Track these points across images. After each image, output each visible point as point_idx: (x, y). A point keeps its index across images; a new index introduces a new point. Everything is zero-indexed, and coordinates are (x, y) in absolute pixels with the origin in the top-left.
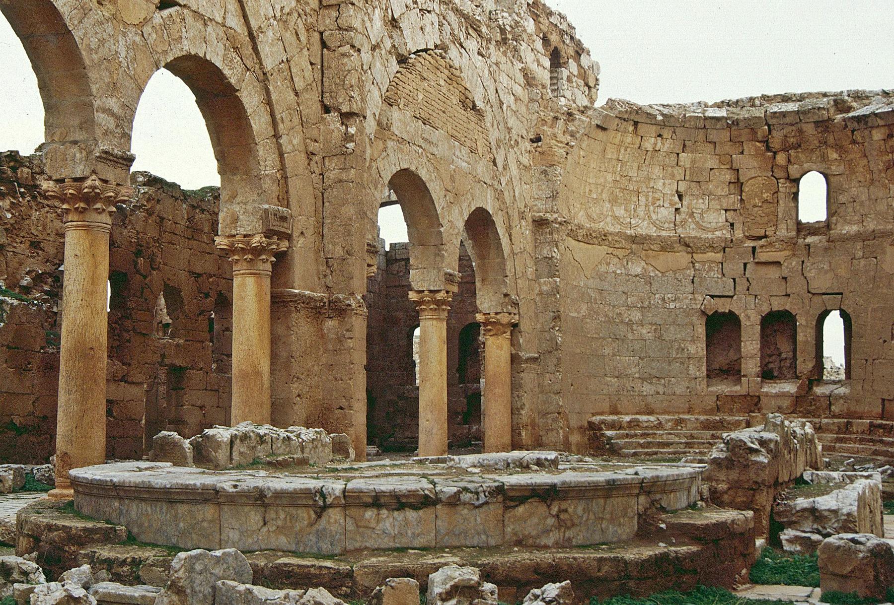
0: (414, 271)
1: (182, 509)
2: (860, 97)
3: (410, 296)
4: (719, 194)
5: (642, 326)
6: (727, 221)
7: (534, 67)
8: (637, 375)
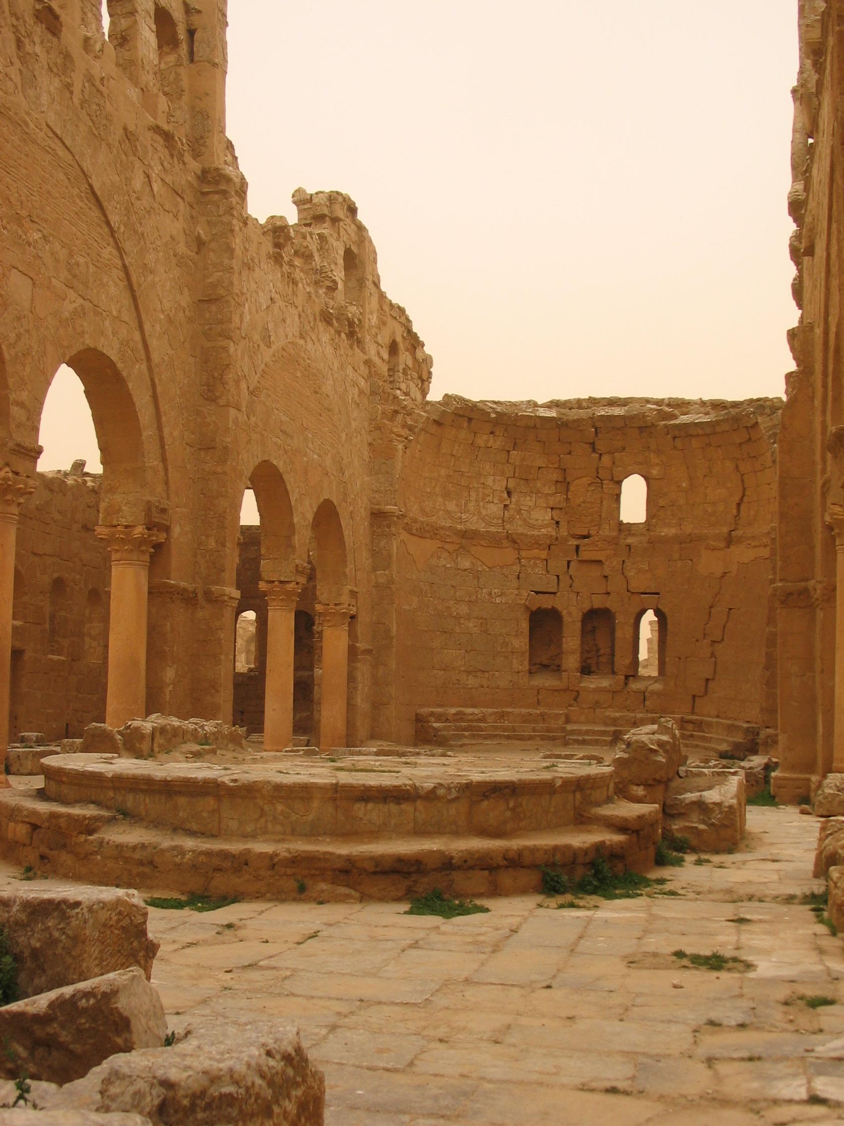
0: (265, 561)
1: (182, 801)
2: (681, 405)
3: (260, 586)
4: (546, 492)
5: (469, 620)
6: (552, 519)
7: (376, 359)
8: (462, 669)
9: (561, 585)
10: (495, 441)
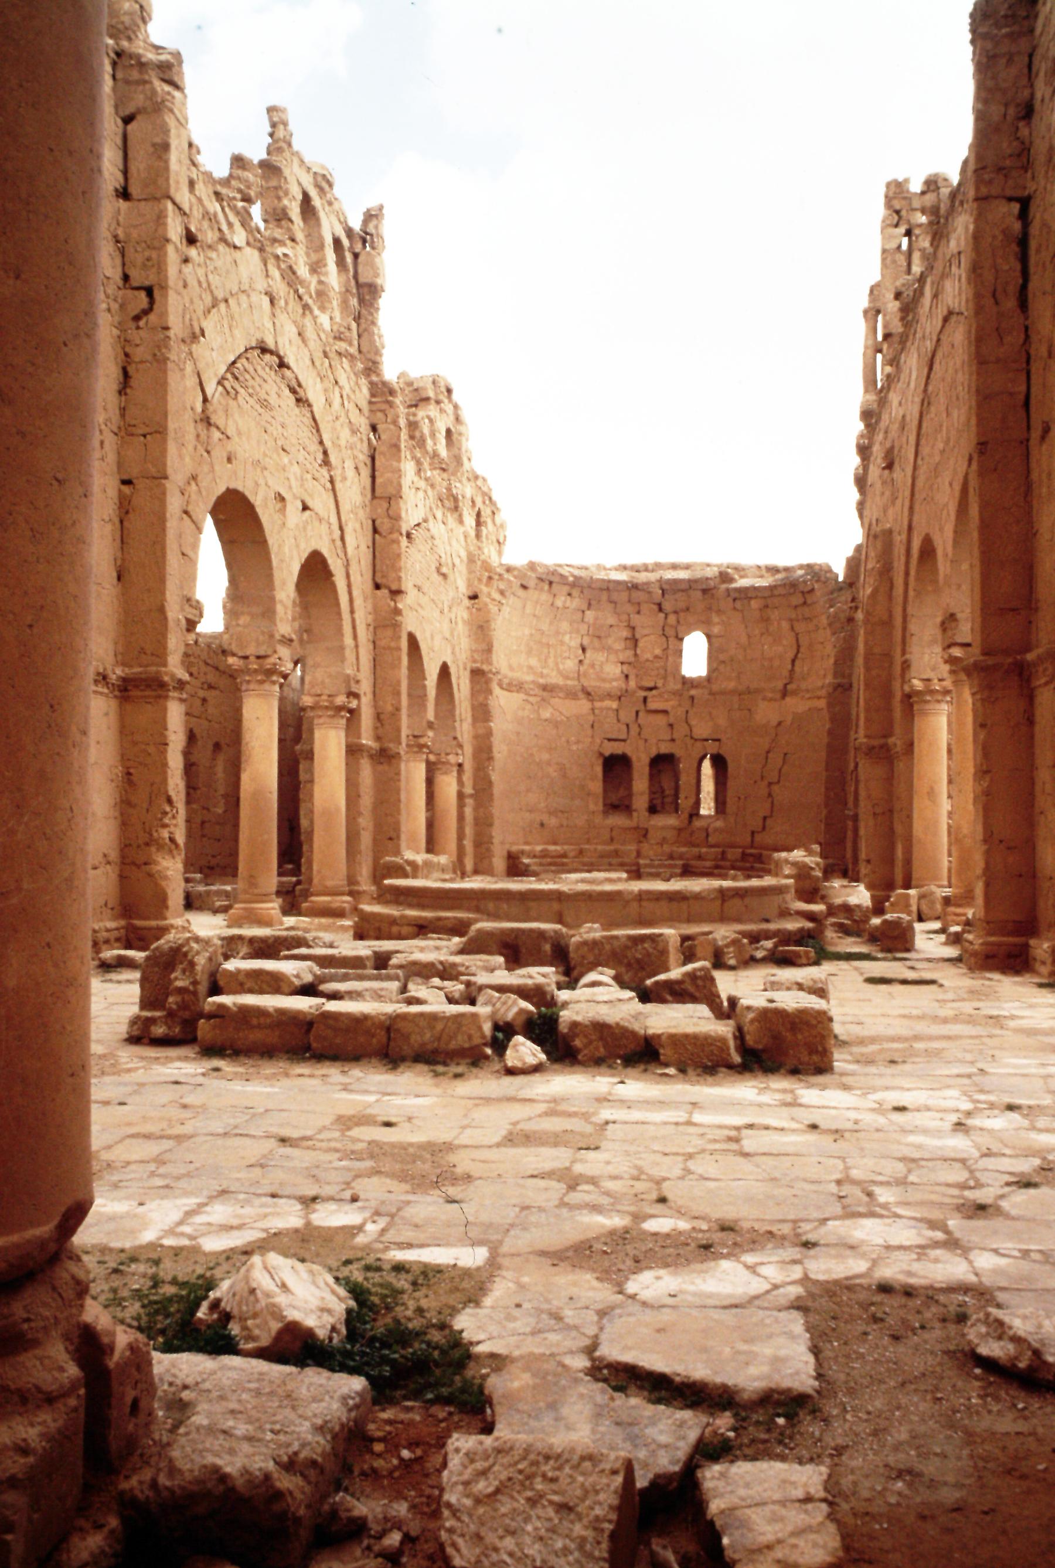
1: (532, 904)
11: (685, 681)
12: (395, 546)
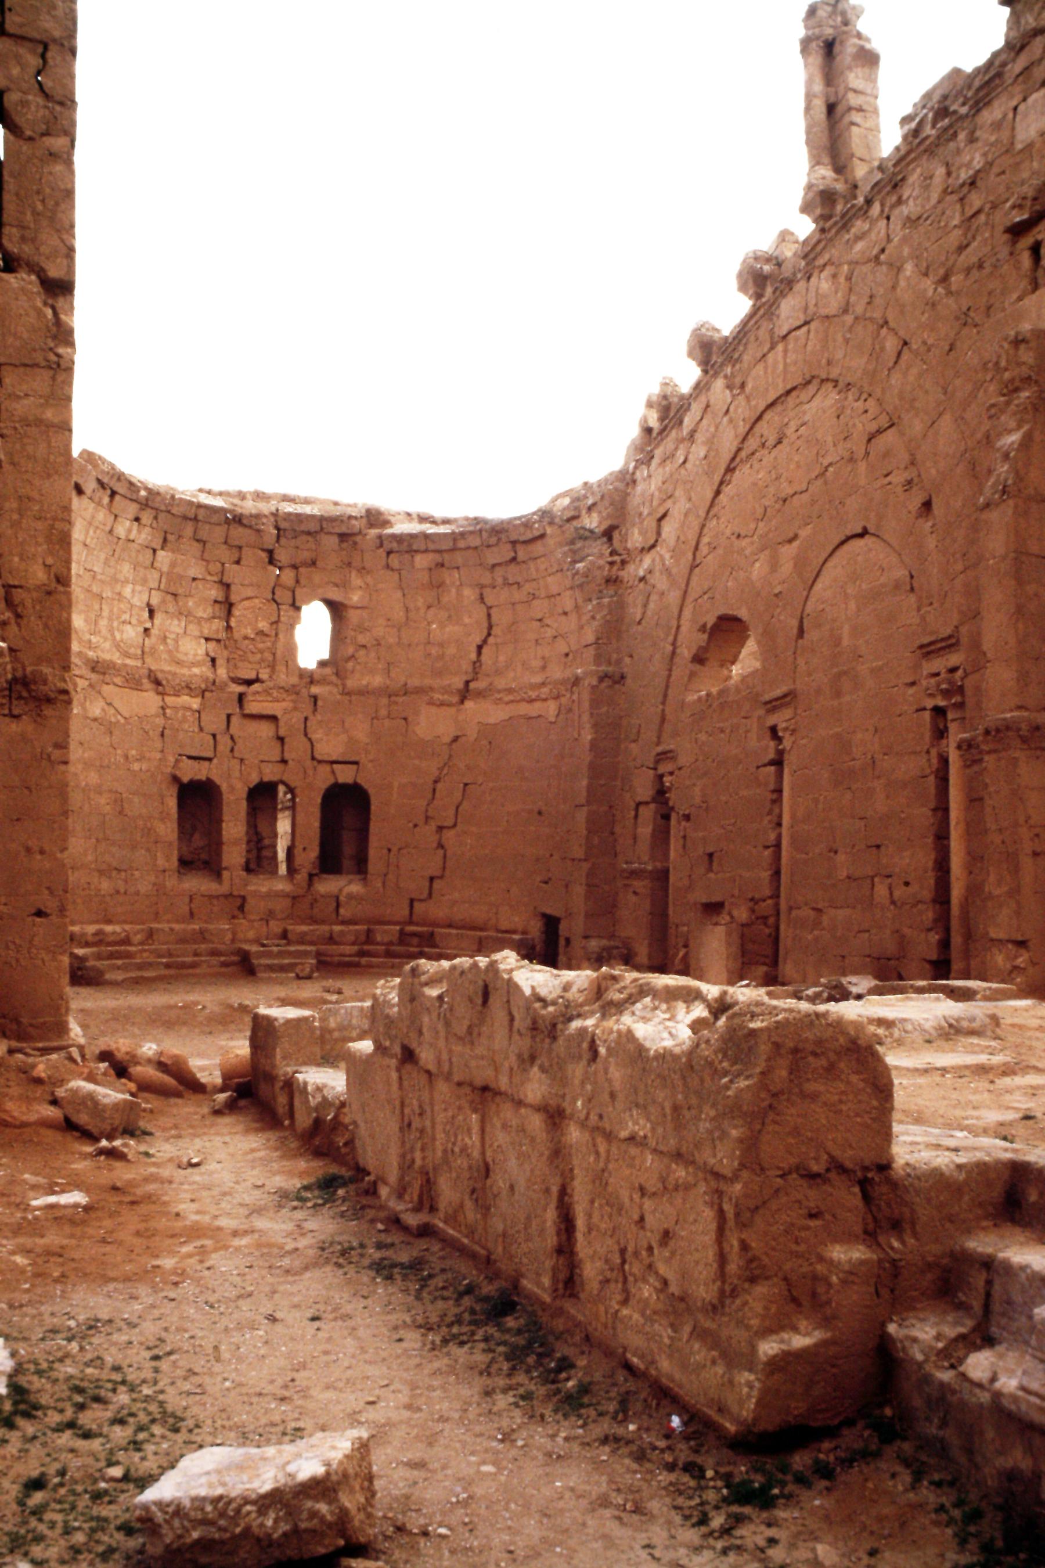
6: (207, 655)
9: (220, 747)
10: (139, 532)
11: (303, 673)
12: (59, 168)
